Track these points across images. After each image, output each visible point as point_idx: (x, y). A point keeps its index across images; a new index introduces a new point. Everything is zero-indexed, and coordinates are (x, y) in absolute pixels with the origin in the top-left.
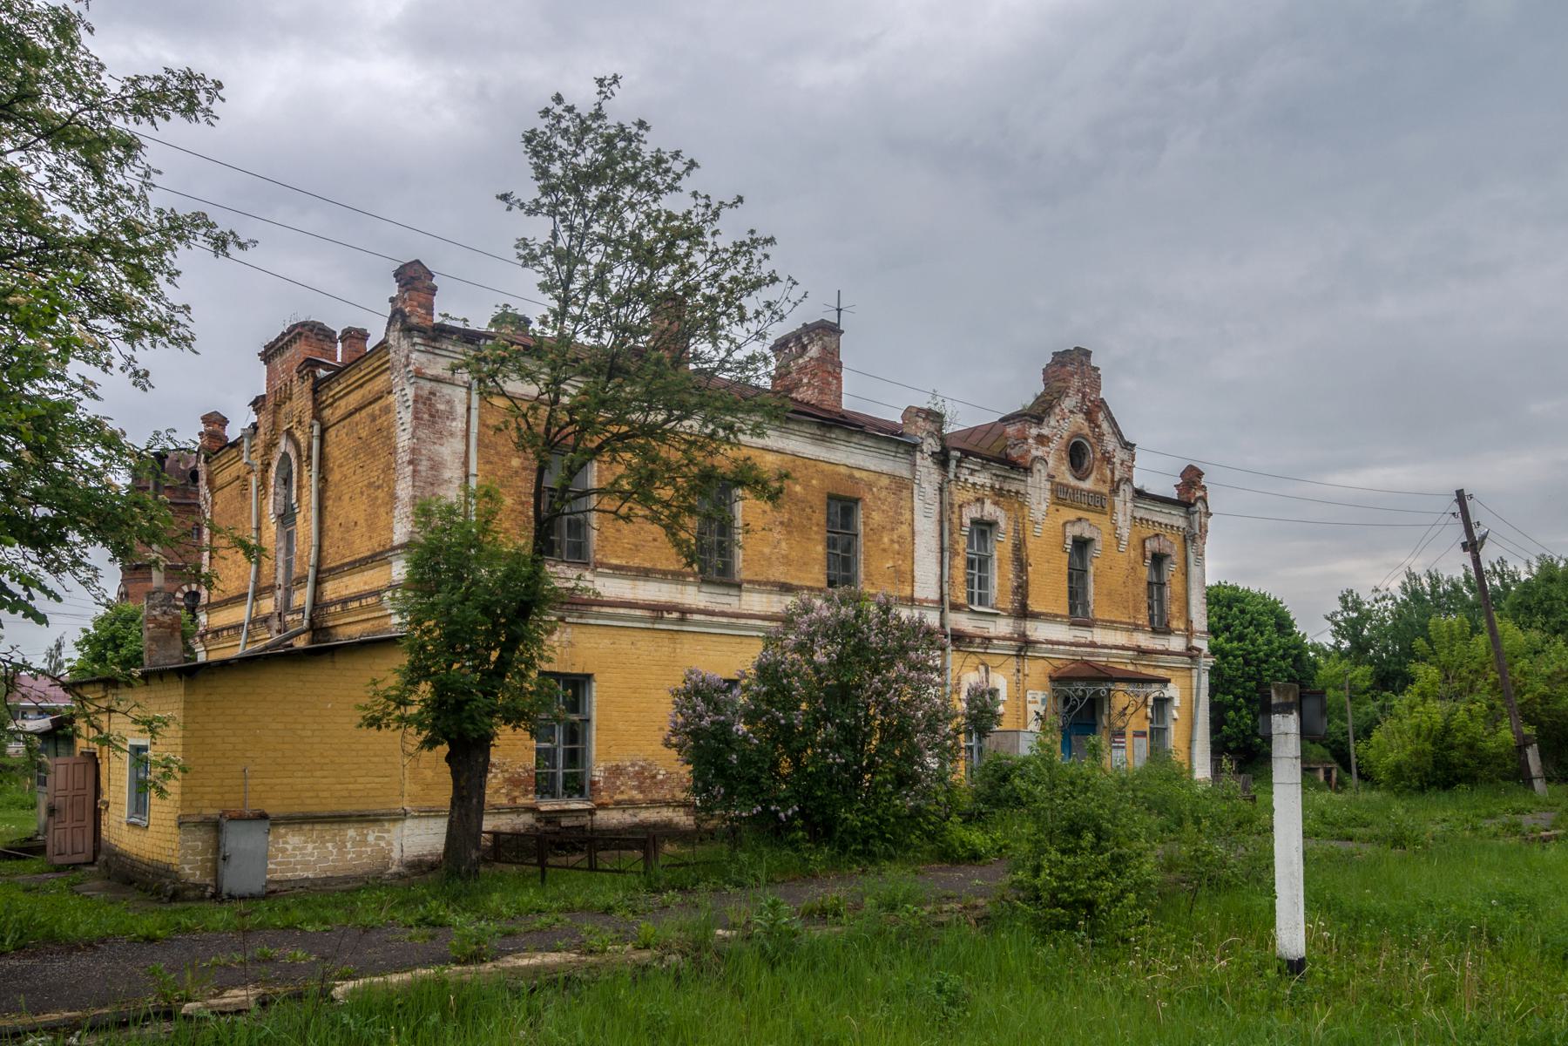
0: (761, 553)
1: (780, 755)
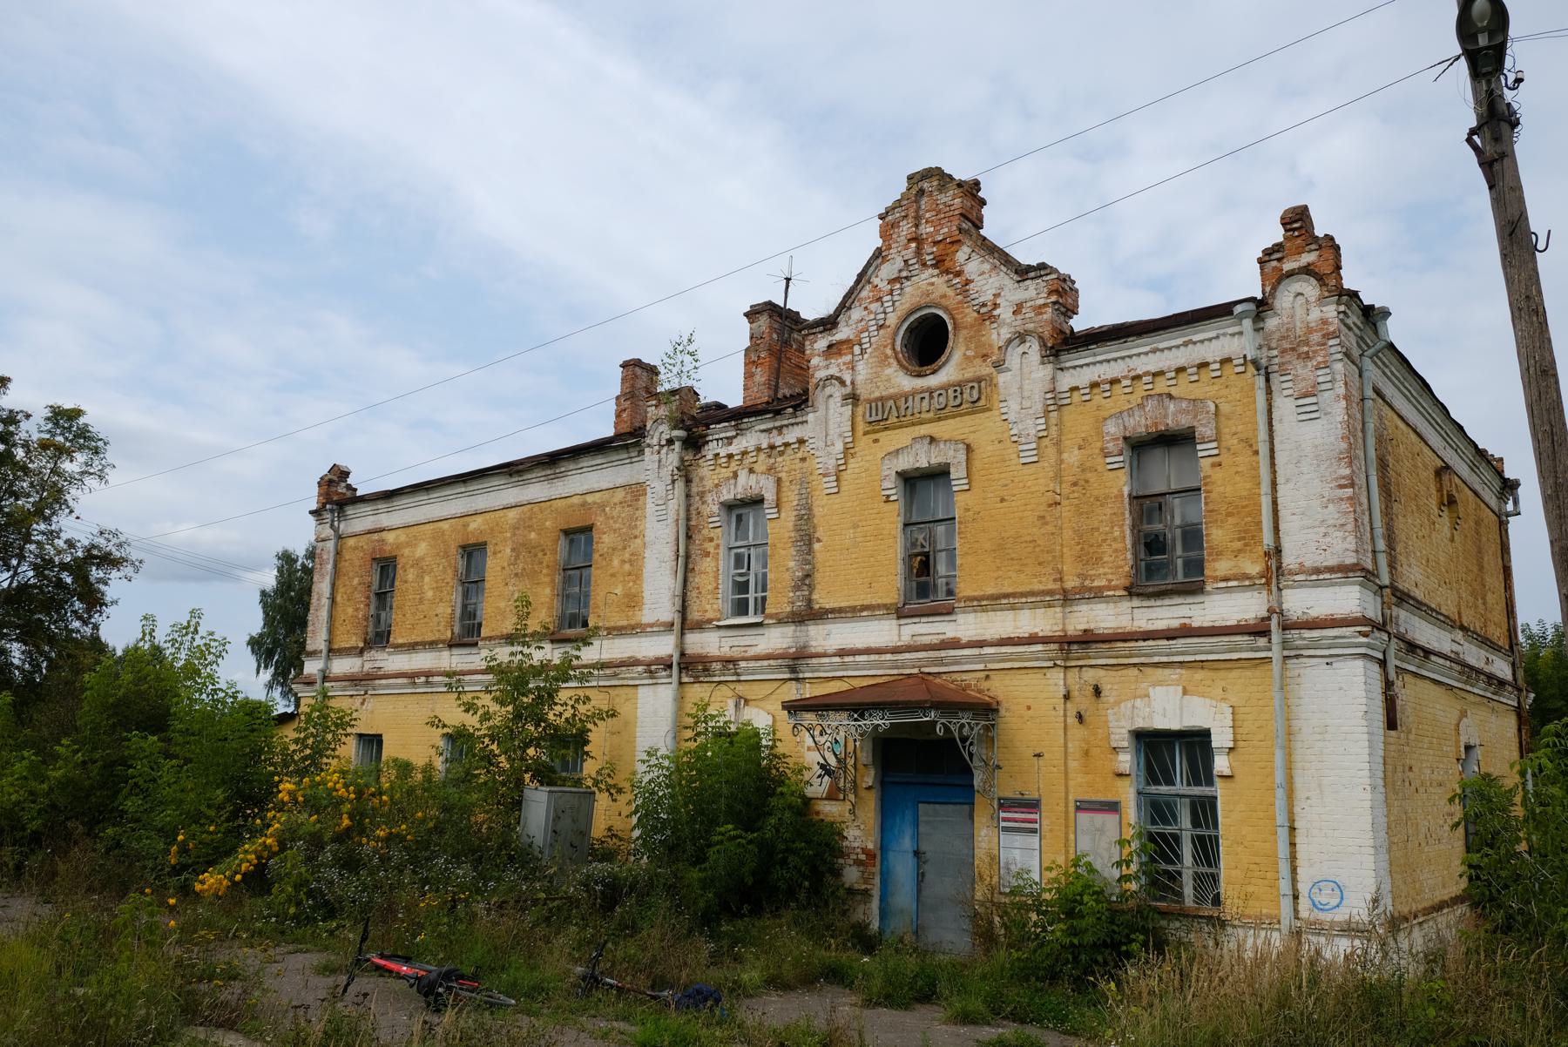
0: (498, 608)
1: (51, 748)
